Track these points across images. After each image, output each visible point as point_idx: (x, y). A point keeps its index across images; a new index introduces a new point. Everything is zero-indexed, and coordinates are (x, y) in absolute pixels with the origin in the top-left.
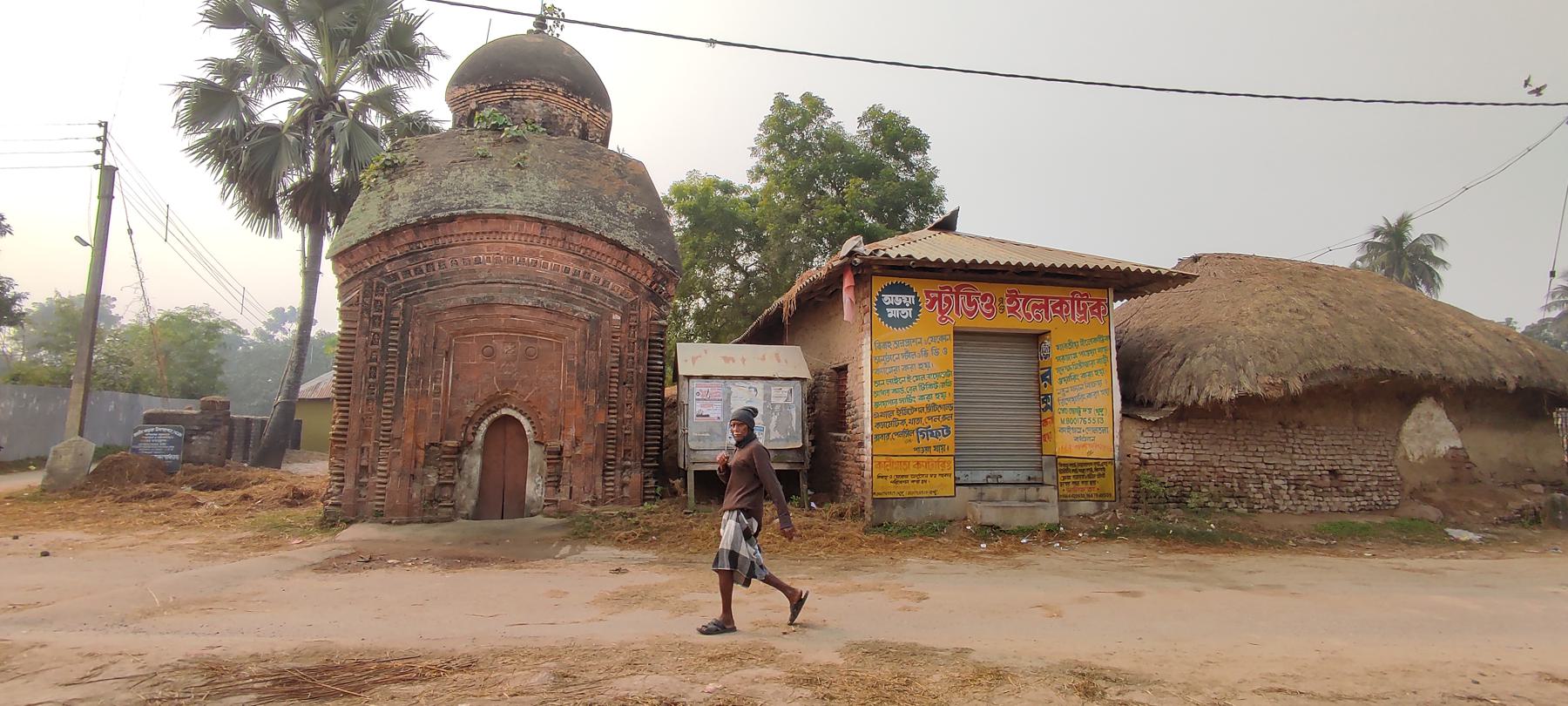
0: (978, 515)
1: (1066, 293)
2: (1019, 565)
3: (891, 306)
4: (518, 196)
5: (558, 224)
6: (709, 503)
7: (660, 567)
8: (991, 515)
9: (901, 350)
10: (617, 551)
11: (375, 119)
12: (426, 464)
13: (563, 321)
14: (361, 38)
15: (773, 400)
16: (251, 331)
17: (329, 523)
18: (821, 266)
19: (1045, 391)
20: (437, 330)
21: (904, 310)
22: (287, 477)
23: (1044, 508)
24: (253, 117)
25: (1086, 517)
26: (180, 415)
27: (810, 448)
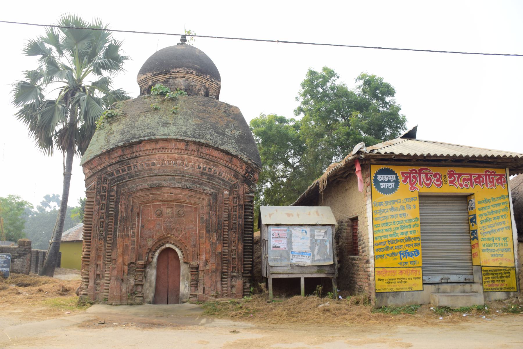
0: (437, 300)
1: (481, 171)
2: (463, 328)
3: (382, 182)
4: (173, 128)
5: (194, 143)
6: (280, 297)
7: (258, 331)
8: (445, 301)
9: (389, 207)
10: (231, 322)
11: (98, 94)
12: (129, 273)
13: (198, 196)
14: (94, 54)
15: (316, 238)
16: (35, 206)
17: (82, 304)
18: (338, 162)
19: (472, 228)
20: (133, 202)
21: (390, 184)
22: (57, 281)
23: (476, 296)
24: (42, 97)
25: (500, 301)
26: (9, 248)
27: (337, 266)
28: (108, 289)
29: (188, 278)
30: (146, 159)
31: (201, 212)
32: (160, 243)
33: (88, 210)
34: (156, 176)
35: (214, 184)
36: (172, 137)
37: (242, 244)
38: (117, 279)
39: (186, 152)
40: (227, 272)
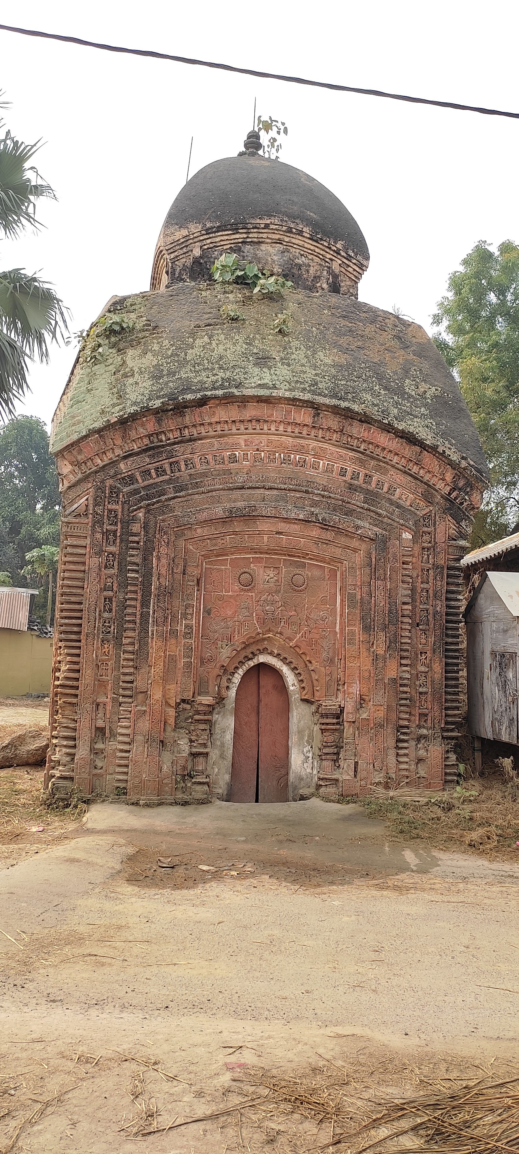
4: (283, 371)
5: (336, 410)
28: (127, 766)
29: (311, 737)
30: (216, 446)
31: (350, 581)
32: (248, 652)
33: (72, 567)
34: (242, 488)
35: (380, 515)
36: (282, 392)
37: (441, 661)
38: (148, 740)
39: (313, 433)
40: (407, 727)
